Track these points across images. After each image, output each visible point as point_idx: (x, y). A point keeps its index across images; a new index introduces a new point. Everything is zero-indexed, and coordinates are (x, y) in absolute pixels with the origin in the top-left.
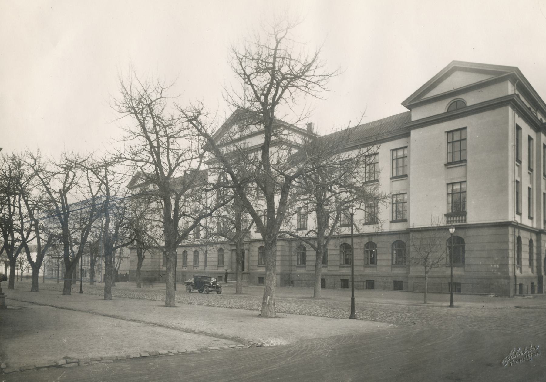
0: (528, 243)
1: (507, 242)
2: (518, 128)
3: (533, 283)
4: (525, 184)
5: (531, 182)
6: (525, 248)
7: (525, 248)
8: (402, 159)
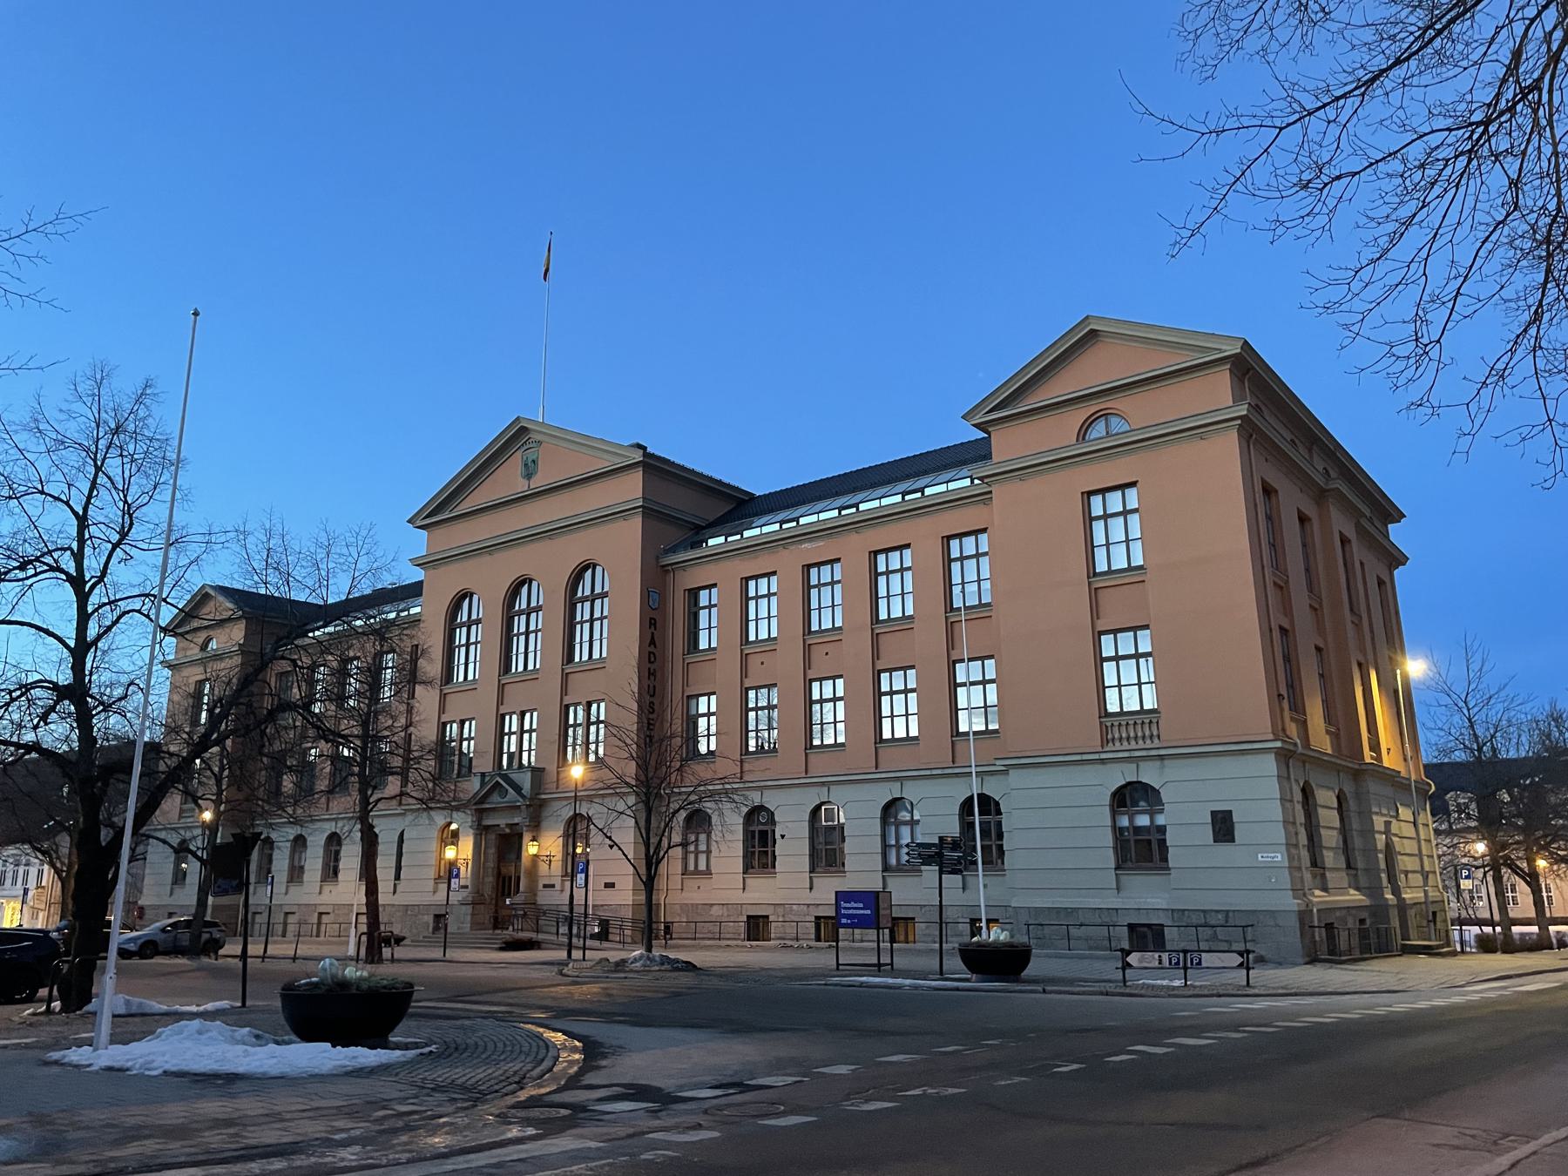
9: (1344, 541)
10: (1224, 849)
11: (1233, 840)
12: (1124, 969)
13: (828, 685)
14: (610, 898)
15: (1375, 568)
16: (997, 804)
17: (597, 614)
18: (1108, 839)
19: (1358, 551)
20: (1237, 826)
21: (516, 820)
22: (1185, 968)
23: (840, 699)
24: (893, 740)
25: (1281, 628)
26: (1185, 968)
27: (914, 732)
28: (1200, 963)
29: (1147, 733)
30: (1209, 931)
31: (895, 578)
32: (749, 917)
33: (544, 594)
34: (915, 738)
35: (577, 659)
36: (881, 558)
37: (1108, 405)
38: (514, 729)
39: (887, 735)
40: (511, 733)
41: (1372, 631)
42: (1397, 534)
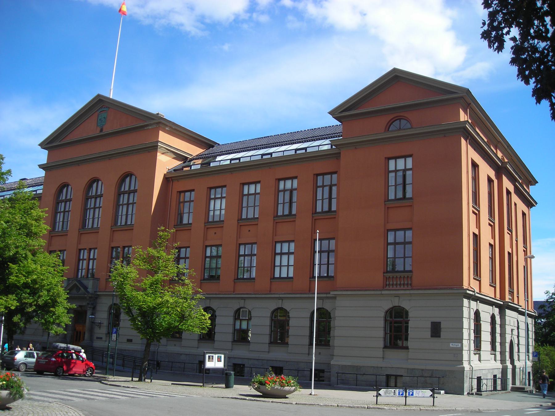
0: (489, 320)
1: (461, 340)
2: (475, 166)
3: (495, 376)
4: (486, 239)
5: (493, 237)
6: (486, 327)
7: (486, 327)
8: (283, 193)
9: (508, 192)
10: (435, 339)
11: (440, 336)
12: (377, 396)
13: (285, 246)
14: (130, 347)
15: (522, 207)
16: (330, 313)
17: (131, 201)
18: (231, 330)
19: (515, 198)
20: (442, 330)
21: (84, 304)
22: (406, 397)
23: (292, 253)
24: (280, 278)
25: (474, 233)
26: (406, 397)
27: (291, 275)
28: (412, 395)
29: (395, 283)
30: (423, 379)
31: (252, 198)
32: (234, 364)
33: (105, 189)
34: (291, 278)
35: (119, 224)
36: (246, 187)
37: (401, 114)
38: (85, 257)
39: (277, 275)
40: (83, 260)
41: (517, 241)
42: (533, 191)
